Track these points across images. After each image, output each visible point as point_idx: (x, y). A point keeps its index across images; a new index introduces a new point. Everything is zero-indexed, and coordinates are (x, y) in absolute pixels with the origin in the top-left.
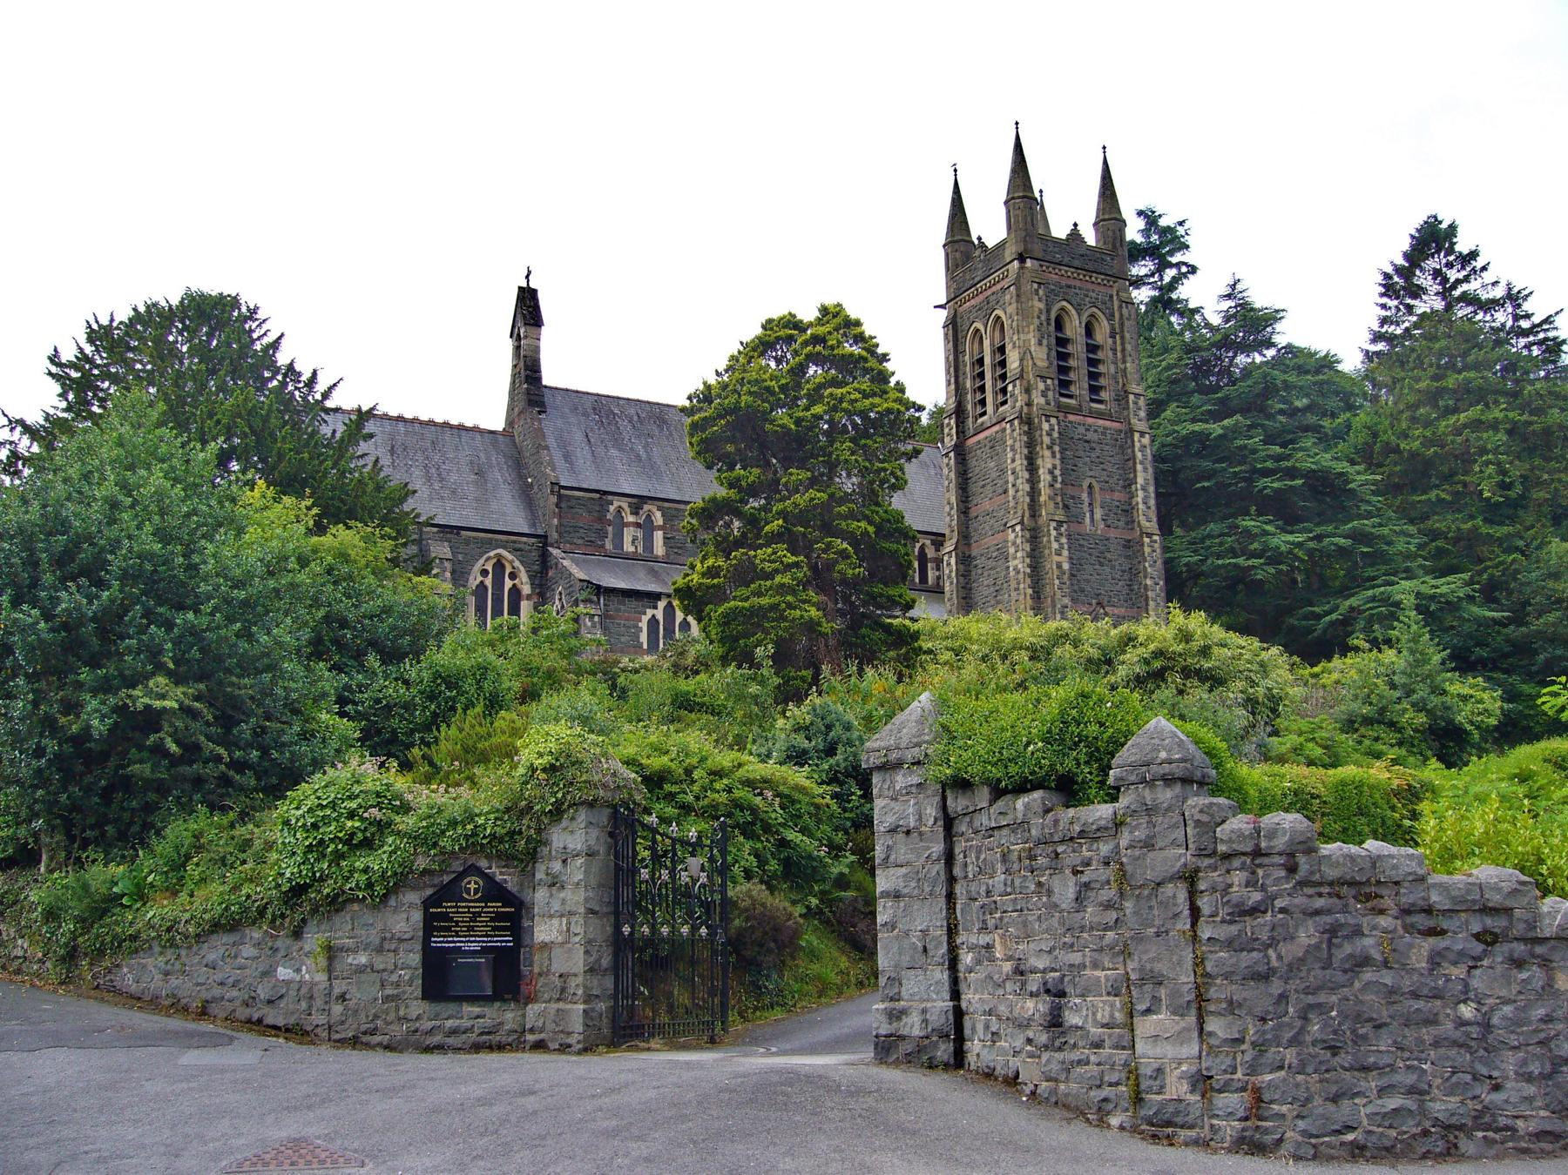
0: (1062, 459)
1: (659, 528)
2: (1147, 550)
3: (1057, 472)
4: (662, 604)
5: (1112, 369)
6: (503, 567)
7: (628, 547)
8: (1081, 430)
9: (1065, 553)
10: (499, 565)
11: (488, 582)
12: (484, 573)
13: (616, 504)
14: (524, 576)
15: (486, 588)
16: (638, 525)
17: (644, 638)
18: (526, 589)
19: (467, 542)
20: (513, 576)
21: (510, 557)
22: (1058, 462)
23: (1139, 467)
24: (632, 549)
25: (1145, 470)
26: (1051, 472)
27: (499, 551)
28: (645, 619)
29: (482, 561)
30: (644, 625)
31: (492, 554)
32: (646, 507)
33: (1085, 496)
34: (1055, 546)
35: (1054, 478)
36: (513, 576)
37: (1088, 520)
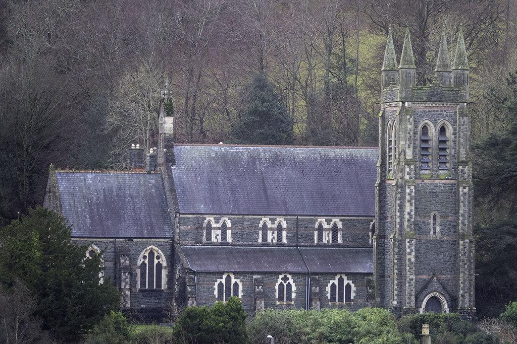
0: (416, 208)
1: (230, 228)
2: (461, 247)
3: (413, 213)
4: (224, 276)
5: (453, 151)
6: (154, 254)
7: (214, 240)
8: (432, 187)
9: (413, 254)
10: (151, 253)
11: (147, 261)
12: (145, 257)
13: (208, 219)
14: (164, 258)
15: (146, 264)
16: (219, 228)
17: (216, 293)
18: (164, 264)
19: (137, 243)
20: (158, 258)
21: (157, 249)
22: (413, 208)
23: (461, 204)
24: (215, 240)
25: (464, 205)
26: (409, 214)
27: (151, 246)
28: (217, 284)
29: (143, 252)
30: (216, 286)
31: (148, 248)
32: (223, 219)
33: (431, 221)
34: (408, 250)
35: (411, 217)
36: (158, 258)
37: (432, 232)
